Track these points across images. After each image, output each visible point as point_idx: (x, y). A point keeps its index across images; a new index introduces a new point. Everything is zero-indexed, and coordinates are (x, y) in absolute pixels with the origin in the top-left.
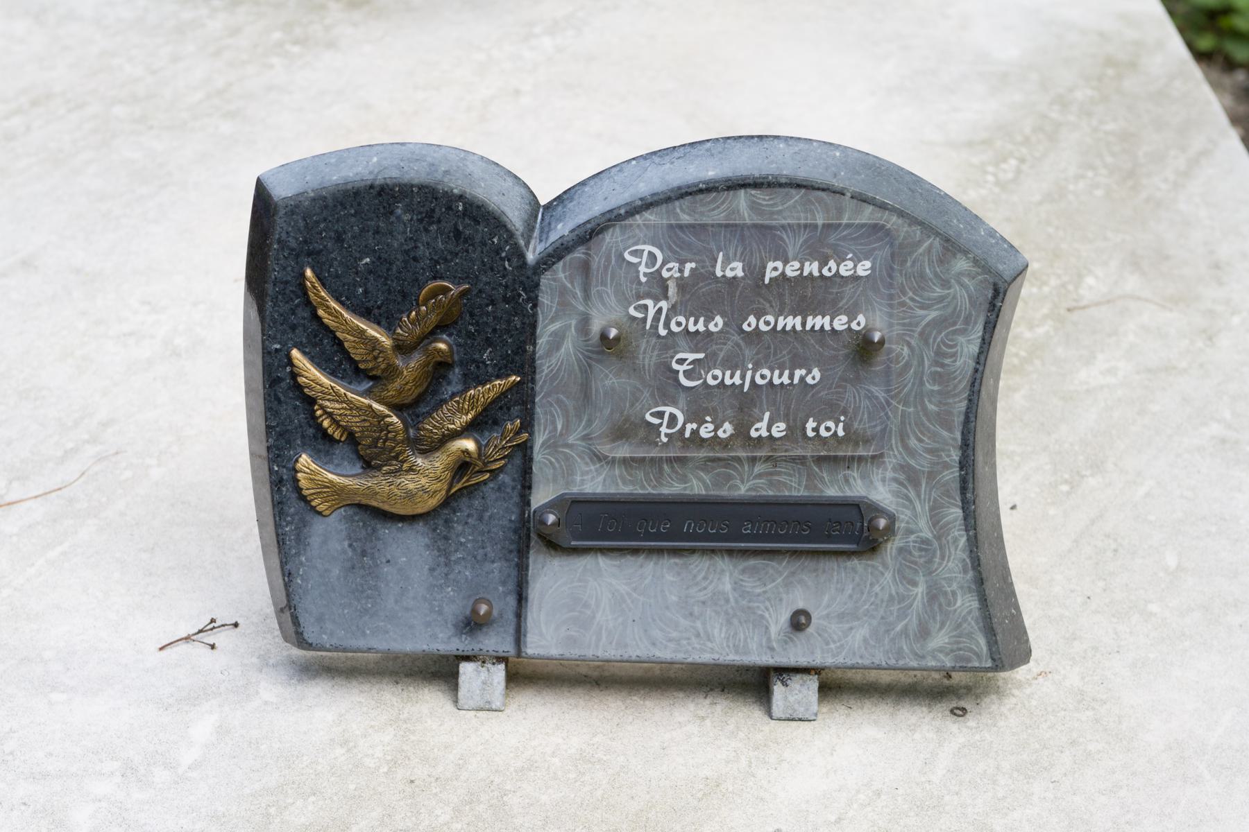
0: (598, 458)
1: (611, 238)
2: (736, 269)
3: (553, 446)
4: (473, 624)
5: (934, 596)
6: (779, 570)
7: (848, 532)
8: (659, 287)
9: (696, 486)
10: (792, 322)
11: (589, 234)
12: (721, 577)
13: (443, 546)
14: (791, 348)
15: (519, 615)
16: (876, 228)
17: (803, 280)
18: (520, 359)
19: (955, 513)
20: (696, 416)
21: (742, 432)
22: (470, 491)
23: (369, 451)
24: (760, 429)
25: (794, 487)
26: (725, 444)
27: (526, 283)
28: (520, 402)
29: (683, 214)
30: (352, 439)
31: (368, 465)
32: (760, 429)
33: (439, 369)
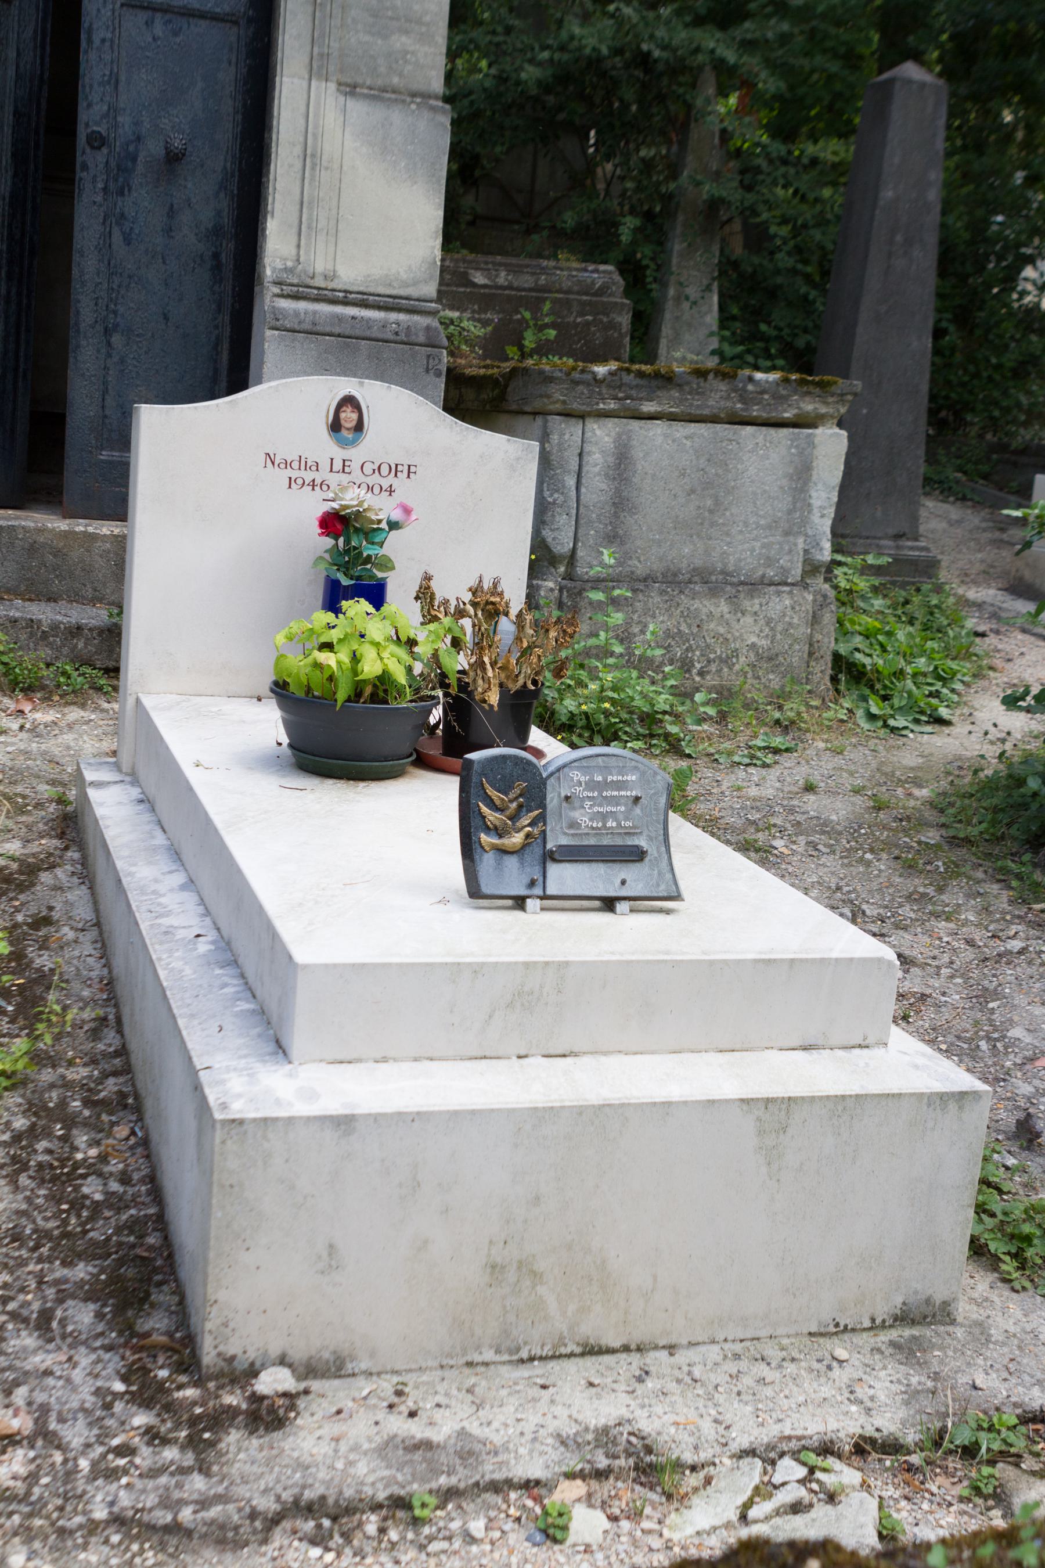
0: (565, 834)
1: (566, 770)
2: (600, 778)
3: (552, 830)
4: (532, 883)
5: (660, 874)
6: (616, 866)
7: (638, 855)
8: (580, 783)
9: (592, 841)
10: (615, 793)
11: (558, 770)
12: (601, 869)
13: (522, 862)
14: (615, 801)
15: (544, 883)
16: (636, 768)
17: (618, 781)
18: (542, 805)
19: (663, 849)
20: (591, 820)
21: (604, 825)
22: (529, 844)
23: (500, 832)
24: (609, 824)
25: (619, 841)
26: (597, 828)
27: (544, 782)
28: (542, 818)
29: (584, 763)
30: (496, 828)
31: (500, 836)
32: (609, 824)
33: (520, 806)
